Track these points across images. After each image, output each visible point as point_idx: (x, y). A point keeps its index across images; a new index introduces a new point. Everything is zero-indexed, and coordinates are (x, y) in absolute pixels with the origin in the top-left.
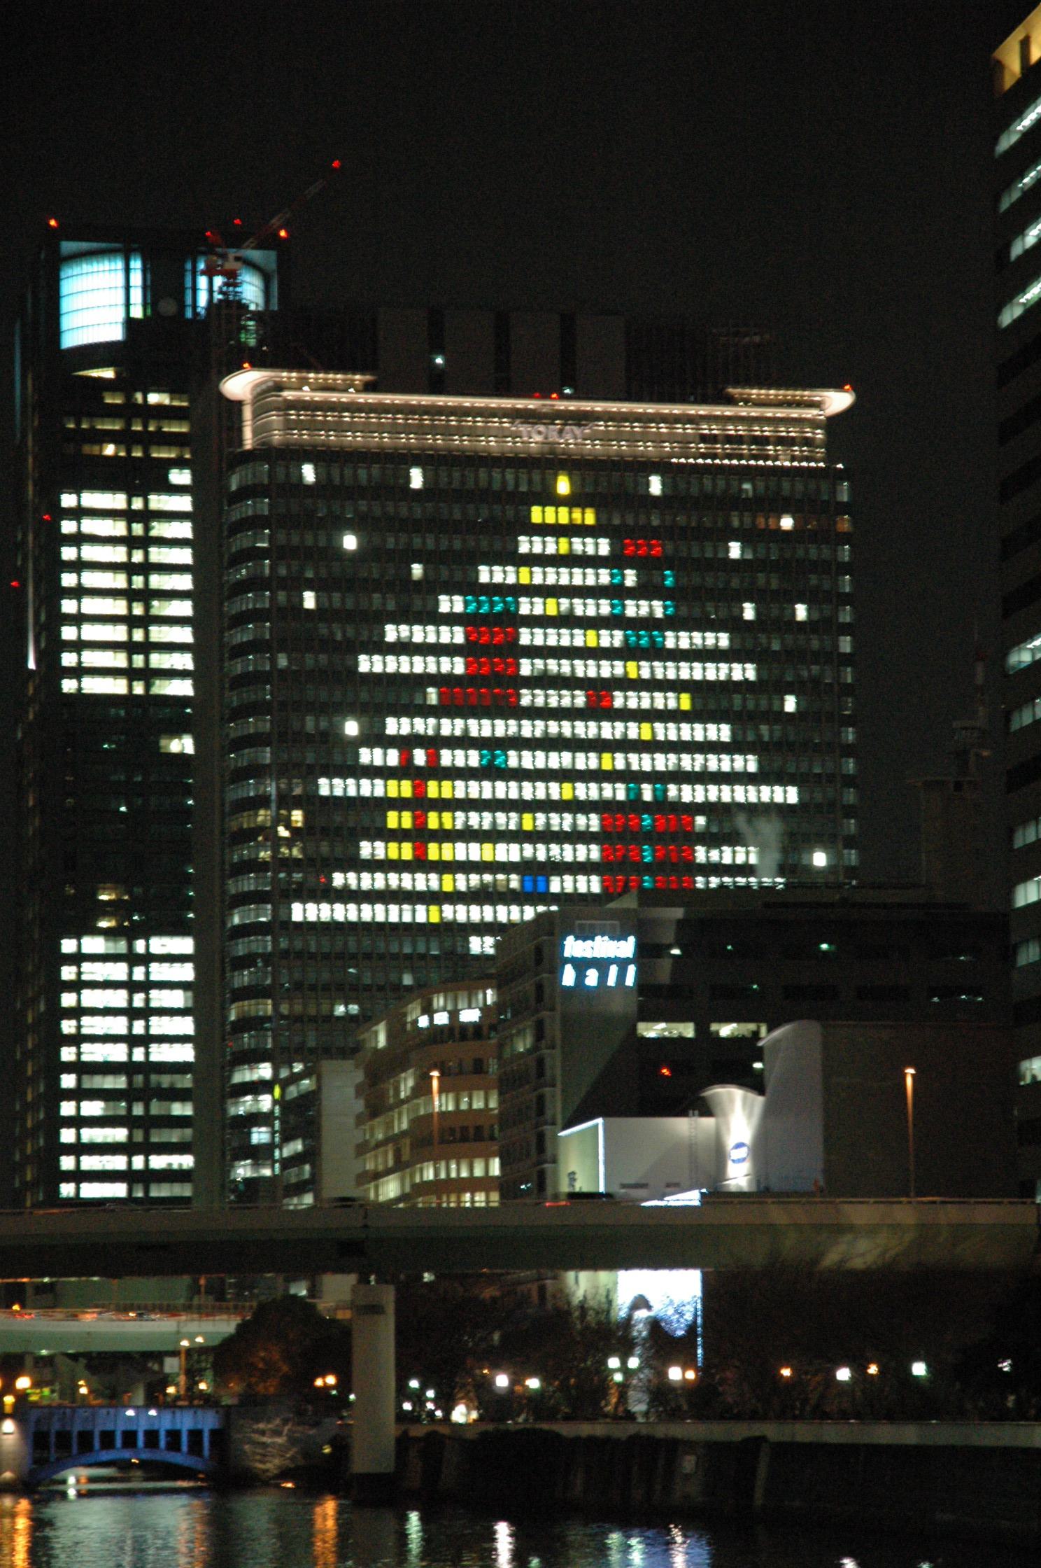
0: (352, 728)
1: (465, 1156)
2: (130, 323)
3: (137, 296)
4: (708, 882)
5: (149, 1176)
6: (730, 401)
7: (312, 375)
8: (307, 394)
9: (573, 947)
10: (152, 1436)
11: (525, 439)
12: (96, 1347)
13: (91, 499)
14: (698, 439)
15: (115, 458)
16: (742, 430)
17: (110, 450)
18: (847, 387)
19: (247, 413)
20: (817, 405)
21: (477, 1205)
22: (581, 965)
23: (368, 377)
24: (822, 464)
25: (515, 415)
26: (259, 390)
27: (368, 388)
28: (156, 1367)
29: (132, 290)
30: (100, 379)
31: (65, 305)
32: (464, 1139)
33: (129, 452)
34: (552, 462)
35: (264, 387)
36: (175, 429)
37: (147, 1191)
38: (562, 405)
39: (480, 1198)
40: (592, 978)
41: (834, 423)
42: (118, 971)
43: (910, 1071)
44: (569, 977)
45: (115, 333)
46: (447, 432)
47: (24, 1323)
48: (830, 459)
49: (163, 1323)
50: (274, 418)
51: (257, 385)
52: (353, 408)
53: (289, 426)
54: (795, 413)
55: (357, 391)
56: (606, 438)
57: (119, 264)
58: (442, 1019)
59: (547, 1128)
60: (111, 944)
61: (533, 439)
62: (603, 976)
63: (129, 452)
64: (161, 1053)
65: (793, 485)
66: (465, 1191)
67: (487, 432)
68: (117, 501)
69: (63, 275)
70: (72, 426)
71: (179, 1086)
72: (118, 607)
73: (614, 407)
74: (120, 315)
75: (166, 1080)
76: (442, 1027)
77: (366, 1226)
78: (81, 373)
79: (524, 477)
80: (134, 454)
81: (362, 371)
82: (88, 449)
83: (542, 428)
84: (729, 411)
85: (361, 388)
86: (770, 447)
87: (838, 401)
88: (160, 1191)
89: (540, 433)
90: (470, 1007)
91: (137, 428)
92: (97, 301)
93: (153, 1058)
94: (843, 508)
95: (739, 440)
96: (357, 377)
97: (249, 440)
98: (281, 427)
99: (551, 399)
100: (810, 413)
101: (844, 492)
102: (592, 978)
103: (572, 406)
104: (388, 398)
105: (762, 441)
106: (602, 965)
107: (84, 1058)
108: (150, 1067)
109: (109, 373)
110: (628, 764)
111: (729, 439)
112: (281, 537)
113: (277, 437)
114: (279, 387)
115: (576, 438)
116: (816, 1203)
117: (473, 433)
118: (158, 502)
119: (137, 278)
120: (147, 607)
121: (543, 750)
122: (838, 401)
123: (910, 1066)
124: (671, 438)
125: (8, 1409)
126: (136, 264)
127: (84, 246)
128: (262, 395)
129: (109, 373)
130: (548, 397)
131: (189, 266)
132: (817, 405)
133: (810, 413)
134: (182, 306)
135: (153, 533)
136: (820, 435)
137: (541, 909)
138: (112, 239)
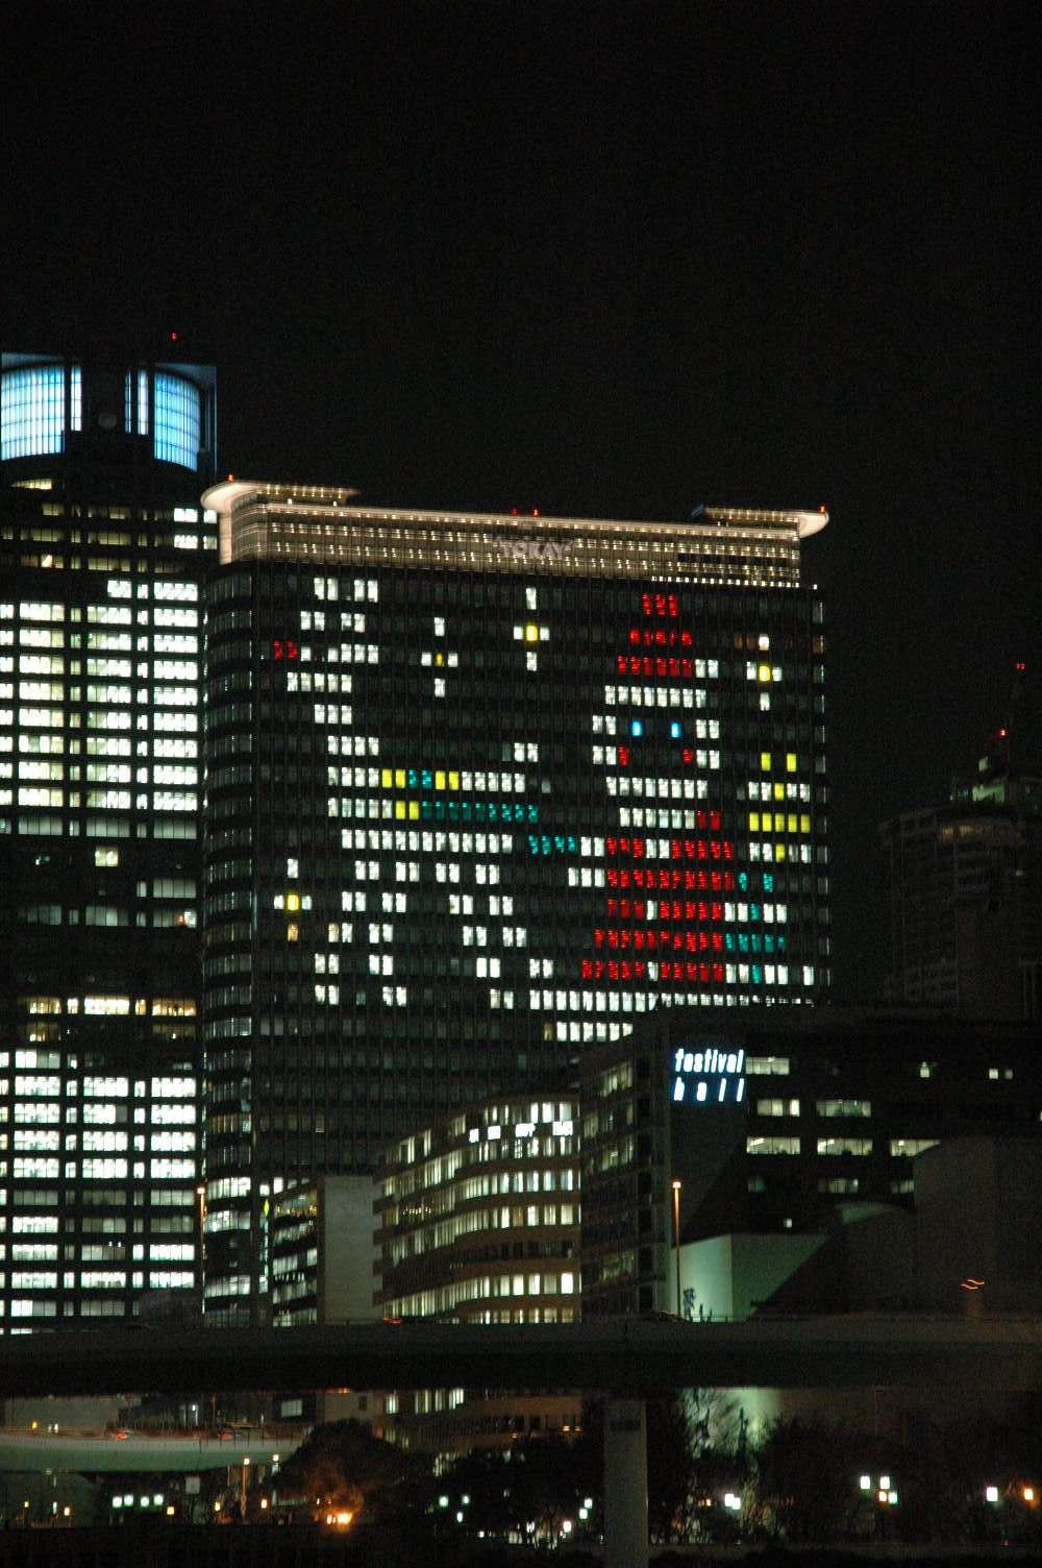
1: (518, 1272)
2: (68, 434)
5: (80, 1294)
6: (706, 520)
7: (295, 489)
8: (290, 507)
9: (686, 1061)
14: (676, 558)
15: (52, 569)
16: (720, 550)
17: (47, 562)
20: (794, 526)
22: (691, 1080)
23: (351, 492)
27: (350, 502)
32: (505, 1256)
33: (67, 564)
34: (523, 578)
36: (114, 542)
37: (77, 1310)
40: (702, 1091)
41: (807, 544)
43: (677, 1185)
45: (54, 446)
48: (805, 579)
50: (255, 529)
52: (337, 522)
53: (272, 538)
54: (770, 535)
55: (339, 505)
56: (585, 555)
57: (60, 377)
59: (655, 1247)
61: (520, 555)
67: (468, 548)
68: (56, 613)
70: (78, 540)
73: (592, 525)
74: (60, 426)
75: (97, 1197)
77: (626, 1340)
79: (465, 591)
81: (345, 486)
82: (25, 561)
83: (523, 545)
84: (707, 531)
85: (344, 501)
87: (812, 522)
88: (89, 1310)
89: (521, 550)
91: (143, 543)
94: (818, 629)
95: (716, 560)
96: (340, 491)
100: (784, 535)
101: (819, 615)
102: (702, 1091)
104: (369, 513)
105: (739, 561)
106: (712, 1079)
108: (81, 1183)
109: (46, 486)
111: (707, 559)
113: (259, 549)
114: (263, 499)
117: (454, 548)
118: (96, 614)
120: (84, 720)
122: (812, 522)
124: (650, 556)
126: (77, 377)
128: (242, 507)
129: (46, 486)
130: (531, 513)
132: (794, 526)
133: (784, 535)
134: (122, 419)
135: (92, 645)
136: (794, 556)
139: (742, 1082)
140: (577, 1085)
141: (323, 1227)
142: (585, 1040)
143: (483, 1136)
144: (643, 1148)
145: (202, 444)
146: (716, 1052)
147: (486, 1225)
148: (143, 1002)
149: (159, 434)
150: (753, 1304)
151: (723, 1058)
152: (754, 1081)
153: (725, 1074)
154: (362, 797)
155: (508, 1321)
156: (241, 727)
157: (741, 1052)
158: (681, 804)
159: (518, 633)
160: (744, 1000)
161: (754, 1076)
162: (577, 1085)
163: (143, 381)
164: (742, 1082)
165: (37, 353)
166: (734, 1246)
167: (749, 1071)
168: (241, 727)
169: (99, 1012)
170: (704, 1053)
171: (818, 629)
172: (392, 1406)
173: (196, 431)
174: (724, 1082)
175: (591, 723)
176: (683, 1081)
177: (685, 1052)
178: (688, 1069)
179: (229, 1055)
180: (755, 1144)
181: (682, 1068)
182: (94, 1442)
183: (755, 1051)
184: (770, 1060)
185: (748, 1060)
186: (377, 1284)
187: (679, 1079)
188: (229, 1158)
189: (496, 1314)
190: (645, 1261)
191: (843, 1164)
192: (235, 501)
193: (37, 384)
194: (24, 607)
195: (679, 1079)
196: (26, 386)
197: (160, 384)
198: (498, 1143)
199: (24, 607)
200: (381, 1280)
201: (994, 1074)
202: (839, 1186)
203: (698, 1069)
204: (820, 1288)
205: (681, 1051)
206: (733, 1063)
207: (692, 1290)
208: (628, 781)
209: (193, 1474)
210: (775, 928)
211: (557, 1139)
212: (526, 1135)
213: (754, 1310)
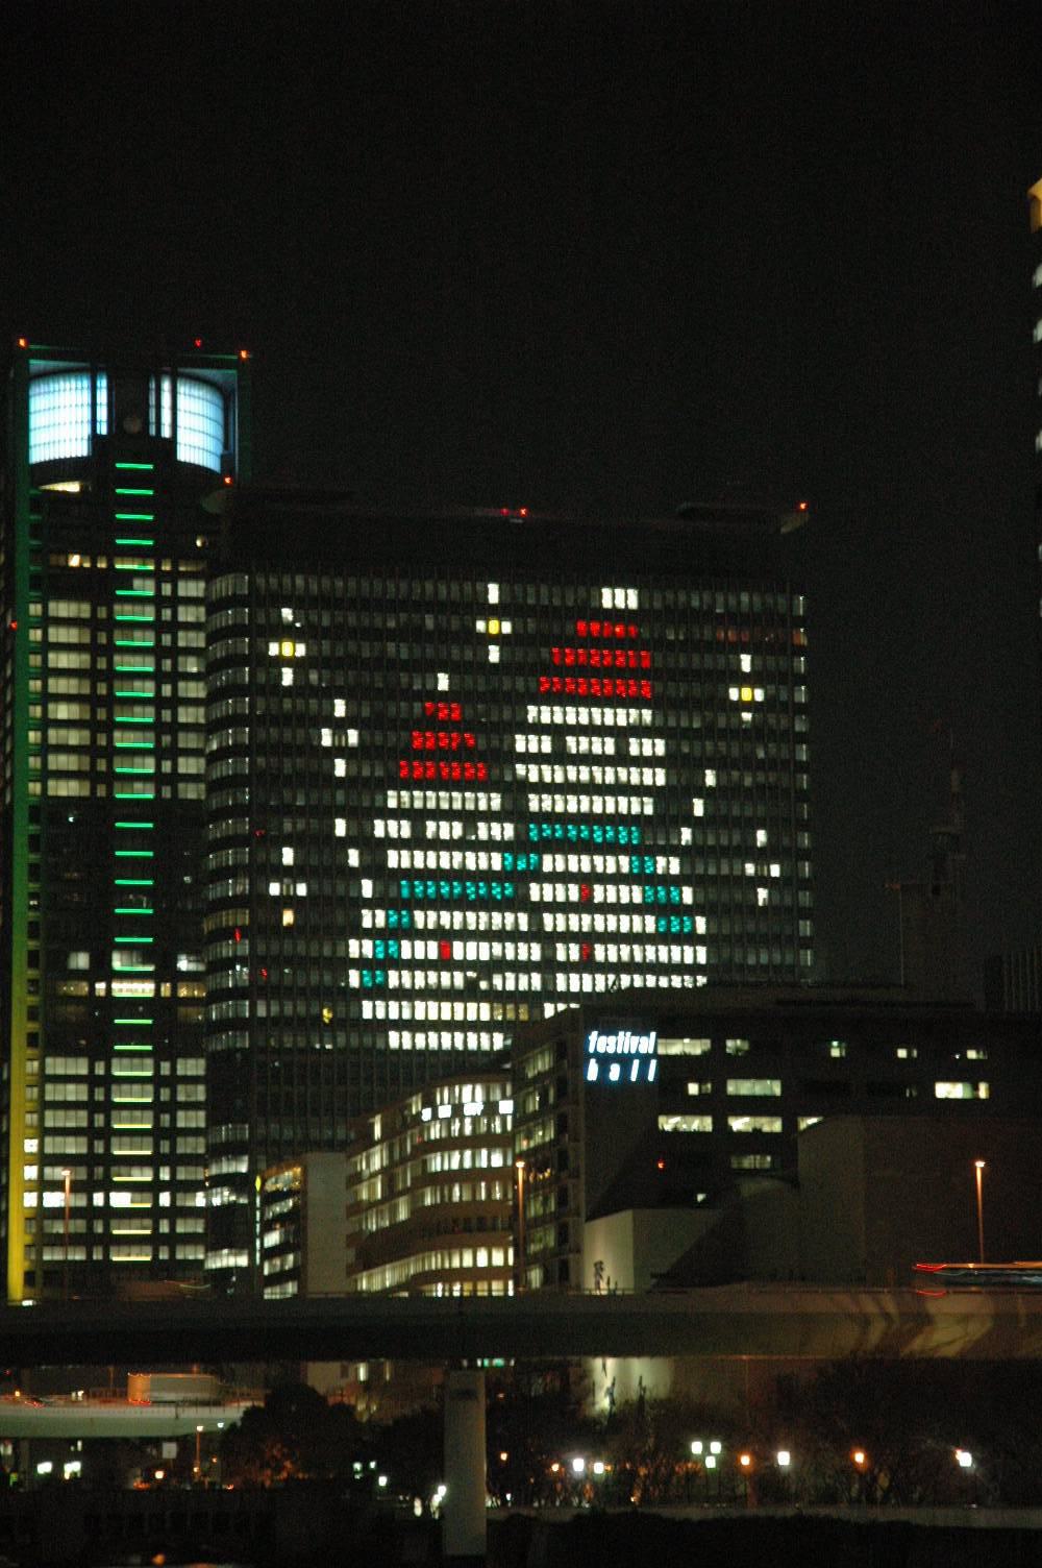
0: (341, 828)
2: (95, 438)
3: (102, 414)
4: (695, 981)
9: (598, 1042)
12: (40, 1433)
15: (81, 567)
21: (494, 1294)
22: (605, 1060)
28: (154, 1452)
29: (98, 407)
30: (65, 493)
33: (94, 563)
39: (497, 1287)
40: (615, 1073)
43: (980, 1164)
44: (593, 1072)
45: (80, 448)
47: (21, 1409)
49: (92, 1409)
57: (86, 383)
62: (625, 1071)
63: (94, 563)
65: (267, 582)
66: (455, 1281)
69: (32, 392)
74: (86, 430)
77: (461, 1313)
80: (99, 566)
92: (63, 419)
102: (615, 1073)
106: (625, 1060)
110: (593, 866)
116: (971, 1292)
119: (102, 397)
121: (421, 850)
123: (981, 1159)
126: (102, 383)
131: (153, 385)
134: (146, 423)
137: (561, 1007)
138: (79, 359)
139: (653, 1063)
140: (508, 1066)
141: (305, 1204)
142: (272, 1014)
143: (435, 1116)
144: (561, 1129)
145: (226, 445)
146: (628, 1034)
147: (439, 1201)
148: (168, 985)
149: (180, 438)
150: (653, 1276)
151: (636, 1039)
152: (666, 1062)
153: (637, 1055)
154: (549, 793)
155: (486, 1294)
156: (235, 721)
157: (653, 1035)
158: (640, 791)
159: (480, 626)
160: (676, 981)
161: (668, 1057)
162: (508, 1066)
163: (166, 385)
164: (653, 1063)
165: (70, 361)
166: (634, 1219)
167: (661, 1051)
168: (235, 721)
169: (125, 994)
170: (617, 1035)
171: (799, 622)
172: (362, 1374)
173: (220, 433)
174: (636, 1063)
175: (527, 712)
176: (597, 1062)
177: (599, 1035)
178: (601, 1050)
179: (228, 1036)
180: (668, 1123)
181: (596, 1049)
182: (75, 1410)
183: (668, 1032)
184: (687, 1041)
185: (660, 1041)
186: (350, 1255)
187: (593, 1062)
188: (227, 1135)
189: (447, 1287)
190: (563, 1236)
191: (755, 1141)
193: (76, 388)
194: (52, 605)
195: (593, 1062)
196: (65, 390)
197: (182, 389)
198: (448, 1122)
199: (52, 605)
200: (354, 1253)
201: (902, 1053)
202: (749, 1162)
203: (611, 1050)
204: (717, 1260)
205: (595, 1034)
206: (646, 1044)
207: (601, 1263)
208: (588, 769)
209: (170, 1439)
210: (490, 906)
211: (504, 1118)
212: (474, 1114)
213: (654, 1281)
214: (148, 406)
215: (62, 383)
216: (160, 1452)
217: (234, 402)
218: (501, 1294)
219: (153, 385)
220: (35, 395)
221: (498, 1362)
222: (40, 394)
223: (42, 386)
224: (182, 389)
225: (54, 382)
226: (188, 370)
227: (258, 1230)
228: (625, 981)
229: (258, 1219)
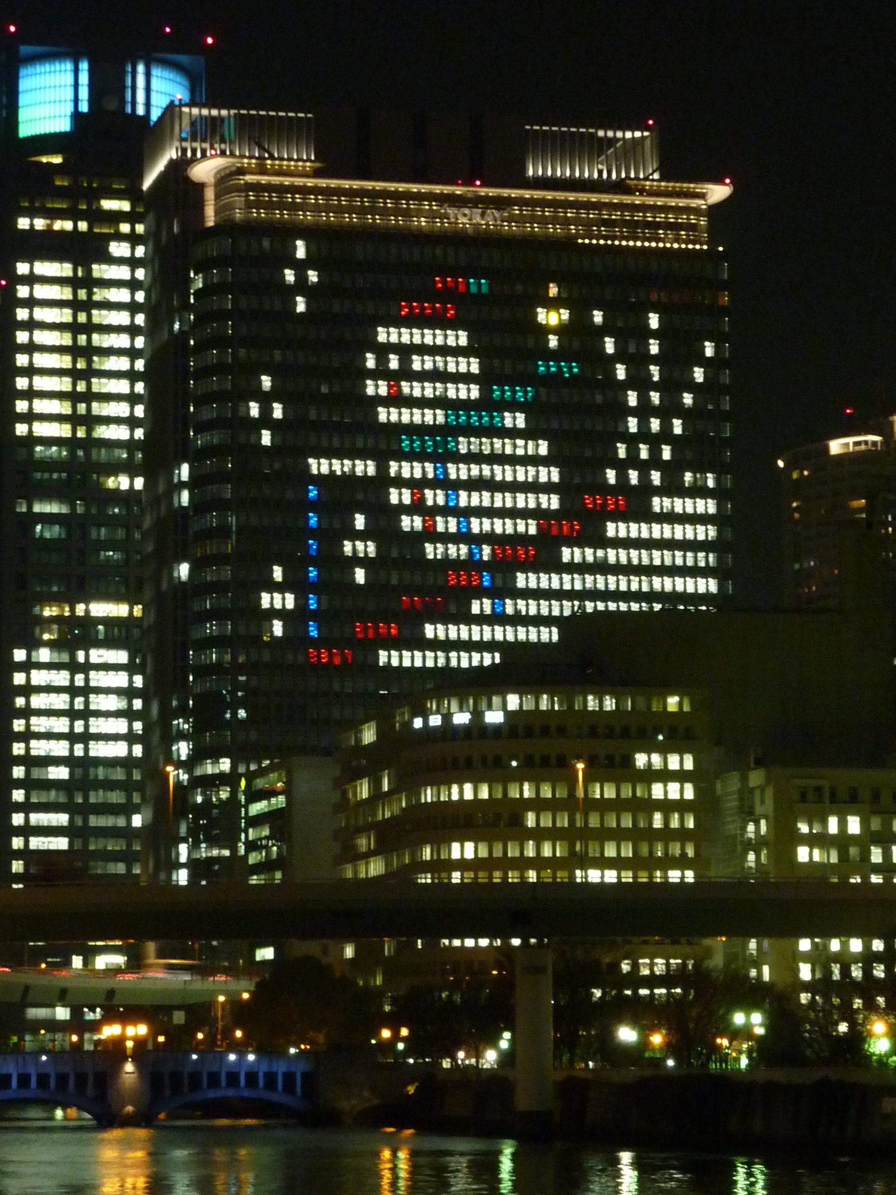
2: (77, 116)
3: (84, 93)
10: (252, 1077)
11: (453, 220)
13: (43, 268)
18: (728, 181)
19: (210, 194)
20: (702, 196)
24: (705, 247)
25: (443, 199)
26: (219, 176)
29: (80, 88)
31: (23, 100)
35: (228, 171)
38: (483, 191)
39: (674, 876)
41: (715, 210)
42: (61, 678)
45: (64, 125)
46: (362, 211)
51: (221, 170)
53: (249, 205)
54: (682, 202)
56: (520, 220)
58: (435, 721)
60: (55, 655)
64: (99, 750)
71: (112, 778)
72: (65, 362)
74: (69, 108)
75: (101, 773)
76: (435, 728)
78: (34, 159)
83: (467, 211)
86: (661, 232)
87: (718, 192)
89: (465, 215)
90: (461, 710)
92: (50, 97)
93: (92, 753)
97: (210, 218)
98: (243, 206)
99: (476, 186)
100: (694, 203)
103: (492, 192)
104: (333, 183)
107: (33, 753)
109: (57, 160)
112: (243, 302)
114: (241, 171)
115: (496, 221)
118: (100, 271)
119: (84, 78)
122: (718, 192)
124: (576, 221)
125: (129, 1052)
126: (84, 66)
127: (38, 49)
128: (224, 180)
129: (57, 160)
132: (702, 196)
133: (694, 203)
138: (59, 45)
163: (141, 68)
192: (216, 174)
197: (156, 72)
209: (179, 1008)
214: (124, 87)
215: (38, 67)
216: (171, 1018)
217: (201, 87)
218: (486, 881)
219: (129, 69)
220: (23, 77)
221: (484, 942)
222: (27, 76)
223: (38, 67)
224: (156, 72)
225: (50, 63)
226: (170, 56)
227: (243, 825)
228: (589, 606)
229: (243, 815)
